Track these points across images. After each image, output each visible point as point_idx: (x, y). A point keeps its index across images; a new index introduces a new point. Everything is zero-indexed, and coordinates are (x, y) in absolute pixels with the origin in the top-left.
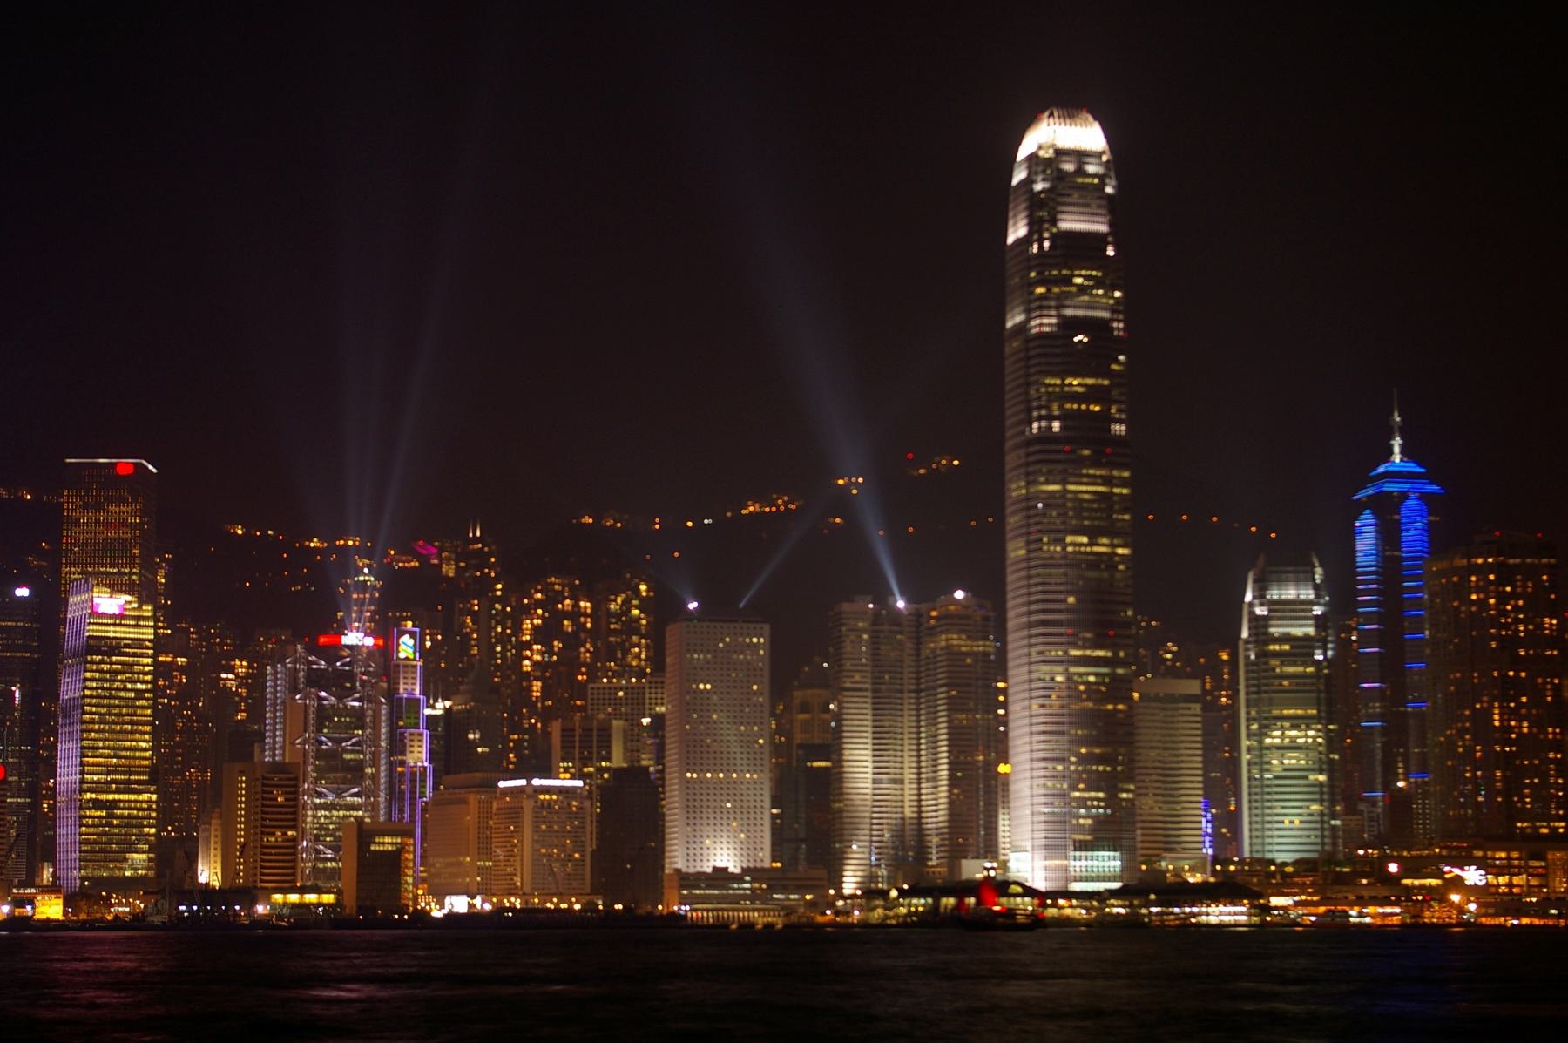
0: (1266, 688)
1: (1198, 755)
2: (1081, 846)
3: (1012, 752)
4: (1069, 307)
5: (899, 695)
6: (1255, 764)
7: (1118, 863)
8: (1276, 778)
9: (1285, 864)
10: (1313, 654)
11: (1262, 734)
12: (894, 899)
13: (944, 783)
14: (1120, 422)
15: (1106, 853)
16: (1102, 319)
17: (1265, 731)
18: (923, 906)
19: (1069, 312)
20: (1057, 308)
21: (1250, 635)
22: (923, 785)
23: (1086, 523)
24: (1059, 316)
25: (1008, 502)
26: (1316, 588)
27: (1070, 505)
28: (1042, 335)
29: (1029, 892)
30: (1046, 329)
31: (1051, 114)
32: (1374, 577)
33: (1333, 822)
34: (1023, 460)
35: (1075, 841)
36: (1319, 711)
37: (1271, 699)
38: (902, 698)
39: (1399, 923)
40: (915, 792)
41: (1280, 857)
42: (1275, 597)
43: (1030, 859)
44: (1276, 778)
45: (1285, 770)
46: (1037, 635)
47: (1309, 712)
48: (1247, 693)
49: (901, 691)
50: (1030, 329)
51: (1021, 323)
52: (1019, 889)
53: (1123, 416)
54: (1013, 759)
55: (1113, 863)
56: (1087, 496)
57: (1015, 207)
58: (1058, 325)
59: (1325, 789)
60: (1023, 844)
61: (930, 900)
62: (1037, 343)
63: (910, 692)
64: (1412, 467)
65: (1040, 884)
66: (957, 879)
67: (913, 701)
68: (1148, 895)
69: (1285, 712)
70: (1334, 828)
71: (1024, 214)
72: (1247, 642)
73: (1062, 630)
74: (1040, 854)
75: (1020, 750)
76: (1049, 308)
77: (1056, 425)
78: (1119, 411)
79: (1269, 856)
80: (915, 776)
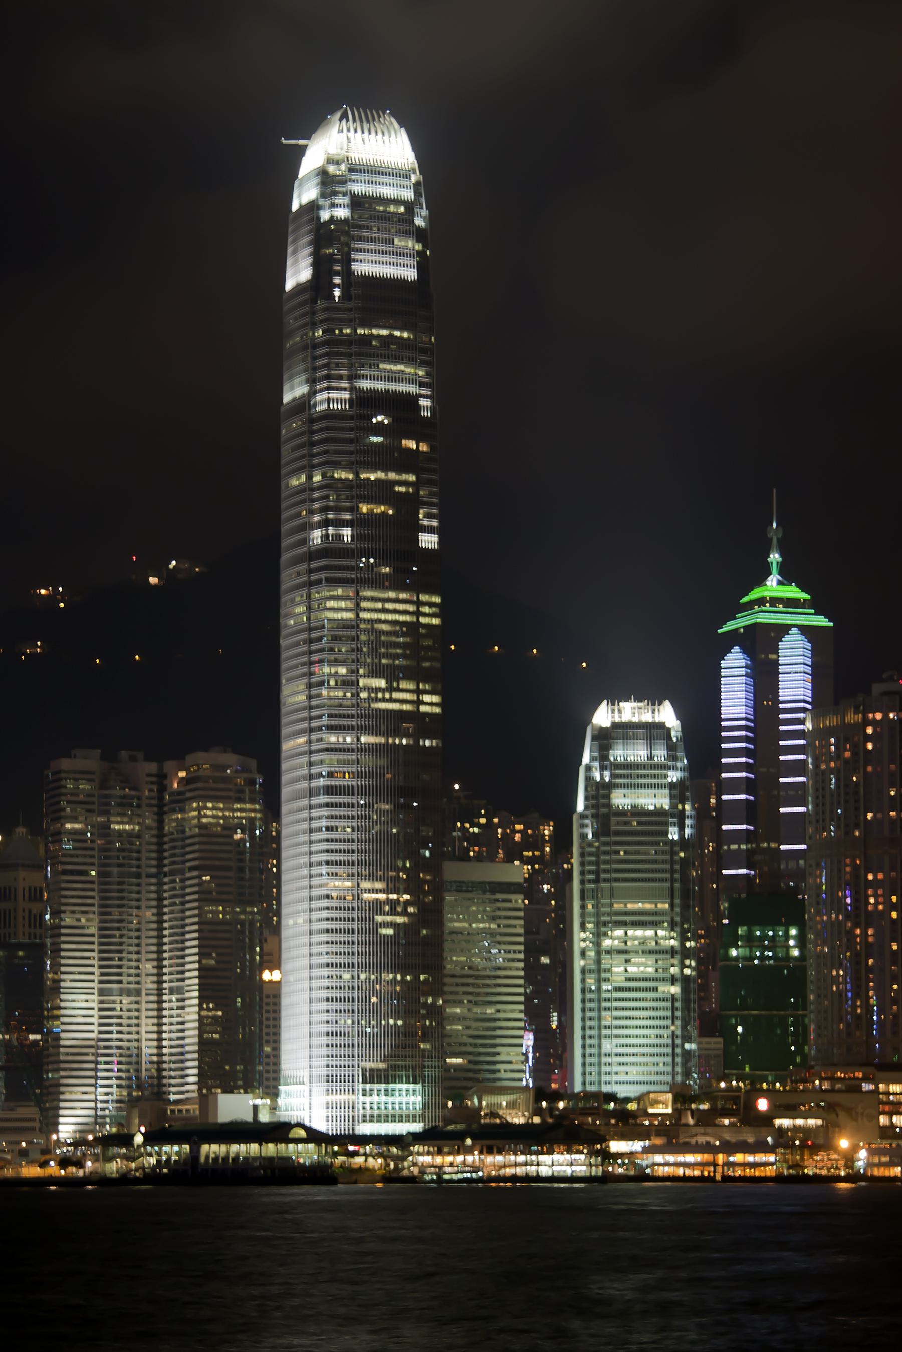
0: (607, 866)
1: (519, 960)
2: (372, 1077)
3: (284, 956)
4: (364, 377)
5: (134, 880)
6: (590, 971)
7: (419, 1098)
8: (617, 989)
9: (628, 1100)
10: (667, 833)
11: (599, 935)
12: (139, 1146)
13: (193, 996)
14: (430, 530)
15: (404, 1086)
16: (408, 395)
17: (603, 929)
18: (177, 1153)
19: (365, 384)
20: (350, 378)
21: (586, 808)
22: (165, 998)
23: (384, 661)
24: (352, 389)
25: (284, 632)
26: (671, 748)
27: (363, 637)
28: (329, 415)
29: (314, 1136)
30: (335, 406)
31: (344, 116)
32: (743, 745)
33: (687, 1046)
34: (304, 578)
35: (364, 1071)
36: (672, 906)
37: (612, 889)
38: (139, 885)
39: (774, 1174)
40: (155, 1006)
41: (623, 1091)
42: (620, 760)
43: (307, 1093)
44: (617, 989)
45: (628, 980)
46: (320, 806)
47: (660, 906)
48: (582, 882)
49: (138, 875)
50: (315, 405)
51: (303, 396)
52: (302, 1133)
53: (435, 523)
54: (284, 966)
55: (412, 1098)
56: (385, 627)
57: (295, 241)
58: (351, 401)
59: (678, 1005)
60: (298, 1073)
61: (186, 1147)
62: (323, 424)
63: (149, 876)
64: (793, 592)
65: (321, 1125)
66: (211, 1120)
67: (153, 888)
68: (463, 1140)
69: (630, 906)
70: (687, 1054)
71: (309, 250)
72: (582, 816)
73: (353, 800)
74: (319, 1088)
75: (295, 953)
76: (340, 378)
77: (347, 533)
78: (429, 516)
79: (606, 1089)
80: (155, 986)
